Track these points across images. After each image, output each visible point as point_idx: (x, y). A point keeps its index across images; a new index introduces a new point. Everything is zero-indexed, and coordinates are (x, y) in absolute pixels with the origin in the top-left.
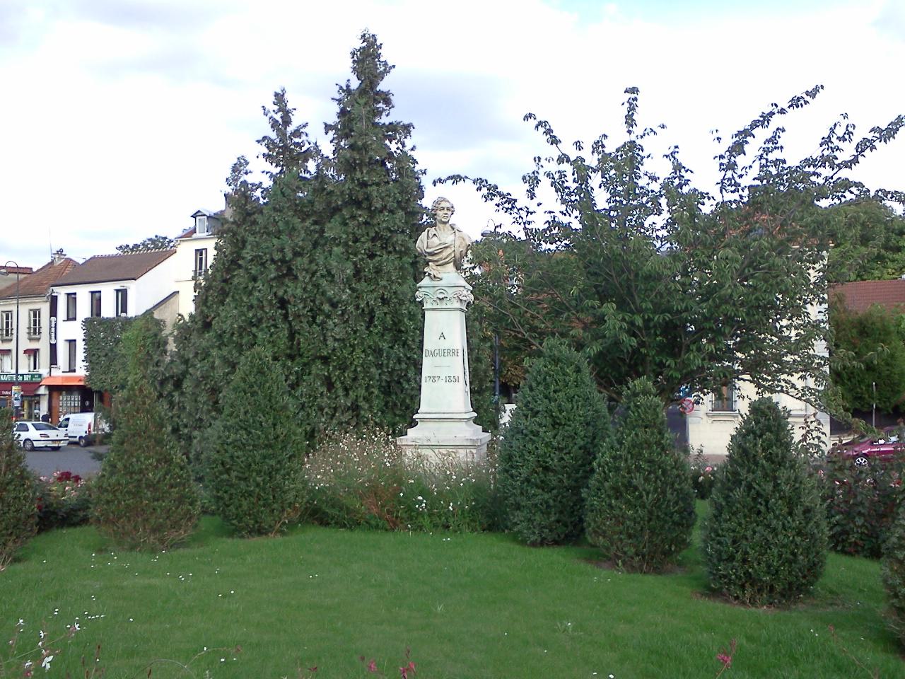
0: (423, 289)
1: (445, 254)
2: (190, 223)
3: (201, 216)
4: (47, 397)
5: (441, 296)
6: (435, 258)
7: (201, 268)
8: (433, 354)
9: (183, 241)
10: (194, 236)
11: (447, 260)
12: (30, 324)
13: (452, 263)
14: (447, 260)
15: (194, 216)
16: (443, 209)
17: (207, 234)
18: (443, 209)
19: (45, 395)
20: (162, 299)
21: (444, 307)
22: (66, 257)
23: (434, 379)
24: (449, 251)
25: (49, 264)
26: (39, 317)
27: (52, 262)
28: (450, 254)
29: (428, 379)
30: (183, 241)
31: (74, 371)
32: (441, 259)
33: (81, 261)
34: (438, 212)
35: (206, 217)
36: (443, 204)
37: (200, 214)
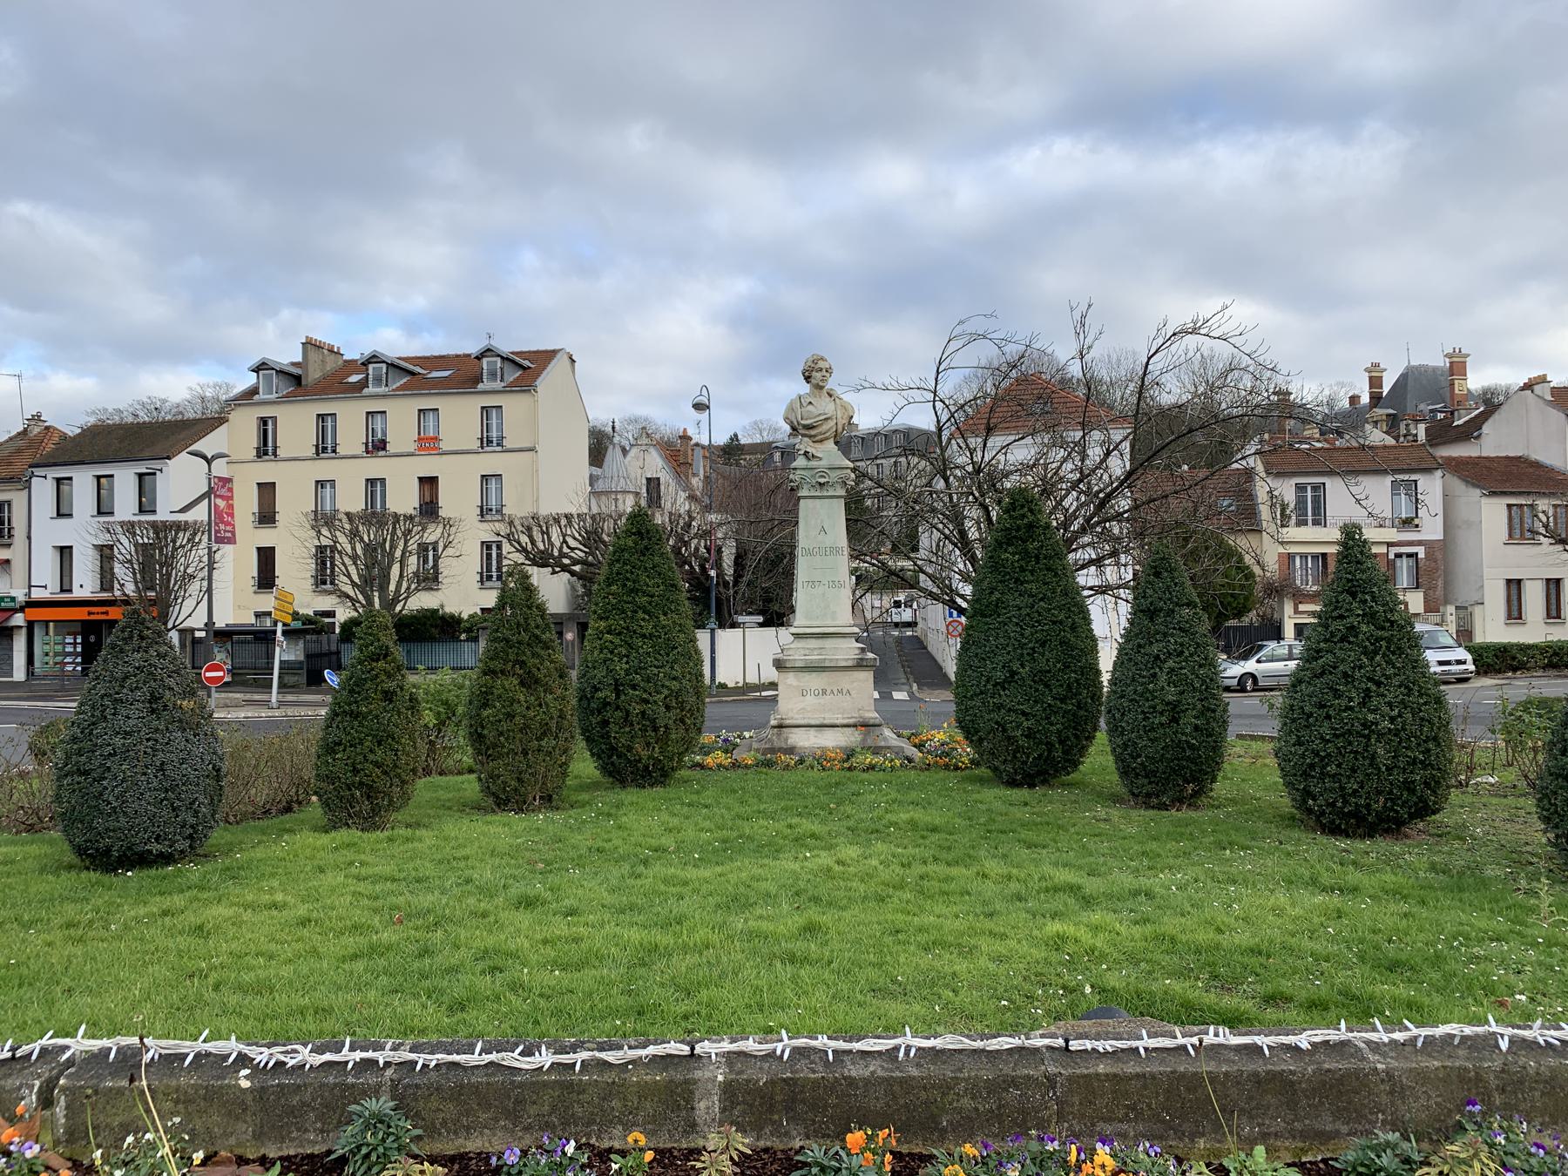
0: (798, 472)
1: (825, 427)
2: (251, 379)
3: (492, 356)
4: (24, 631)
5: (822, 480)
6: (813, 432)
7: (265, 444)
8: (810, 553)
9: (240, 405)
10: (366, 391)
11: (827, 435)
12: (482, 568)
13: (832, 440)
14: (827, 435)
15: (257, 370)
16: (821, 370)
17: (277, 395)
18: (821, 370)
19: (21, 627)
20: (1506, 520)
21: (825, 494)
22: (46, 424)
23: (812, 583)
24: (831, 423)
25: (19, 434)
26: (9, 512)
27: (25, 430)
28: (832, 428)
29: (805, 584)
30: (240, 405)
31: (70, 591)
32: (821, 434)
33: (72, 431)
34: (814, 374)
35: (384, 366)
36: (821, 364)
37: (489, 354)
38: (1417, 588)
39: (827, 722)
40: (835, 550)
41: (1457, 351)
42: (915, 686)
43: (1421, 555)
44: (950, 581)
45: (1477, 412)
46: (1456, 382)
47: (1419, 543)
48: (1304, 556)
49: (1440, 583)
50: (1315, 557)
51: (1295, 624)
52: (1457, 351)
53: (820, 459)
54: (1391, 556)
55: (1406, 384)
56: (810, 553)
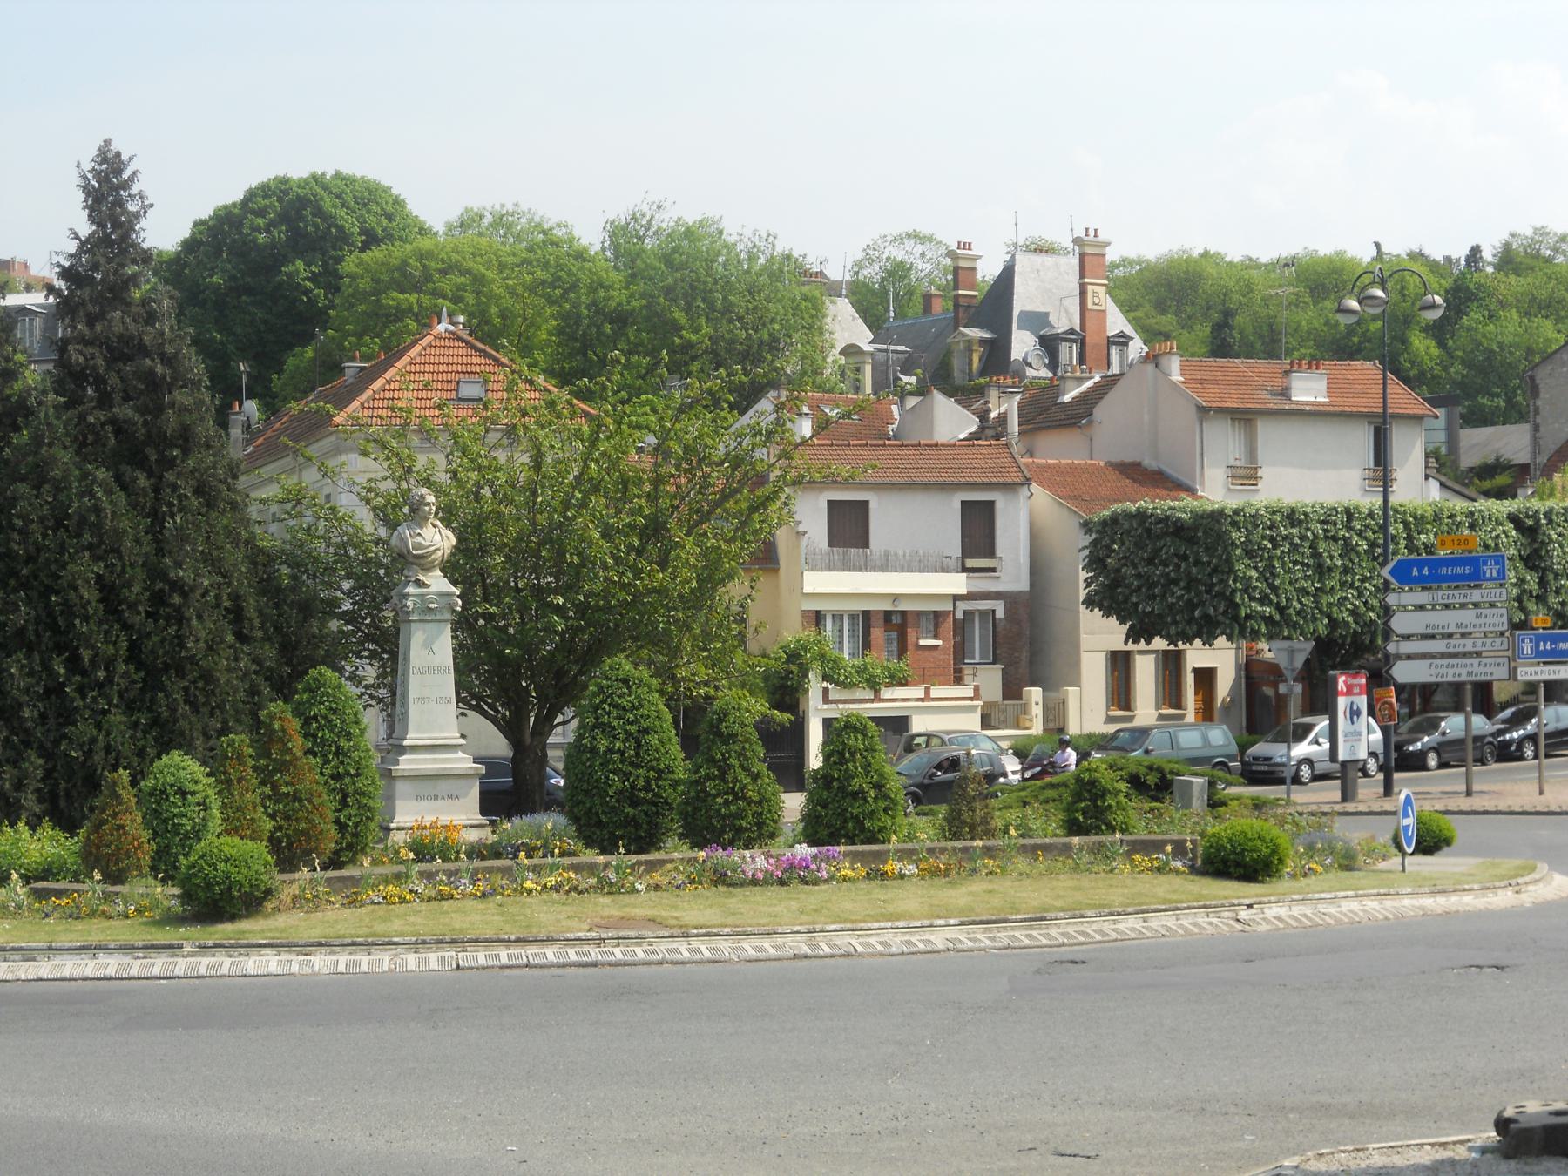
8: (420, 671)
23: (422, 699)
38: (994, 663)
39: (1528, 808)
40: (444, 670)
41: (1092, 233)
42: (99, 772)
43: (1000, 614)
44: (98, 516)
45: (1090, 383)
46: (1089, 287)
47: (997, 596)
48: (837, 617)
49: (1025, 656)
50: (853, 617)
51: (831, 504)
52: (1092, 233)
53: (428, 586)
54: (960, 615)
55: (1013, 266)
56: (420, 671)
